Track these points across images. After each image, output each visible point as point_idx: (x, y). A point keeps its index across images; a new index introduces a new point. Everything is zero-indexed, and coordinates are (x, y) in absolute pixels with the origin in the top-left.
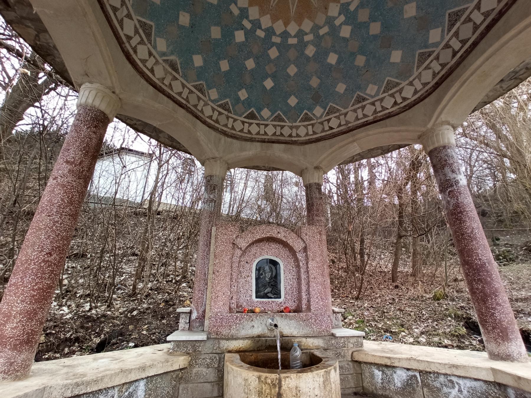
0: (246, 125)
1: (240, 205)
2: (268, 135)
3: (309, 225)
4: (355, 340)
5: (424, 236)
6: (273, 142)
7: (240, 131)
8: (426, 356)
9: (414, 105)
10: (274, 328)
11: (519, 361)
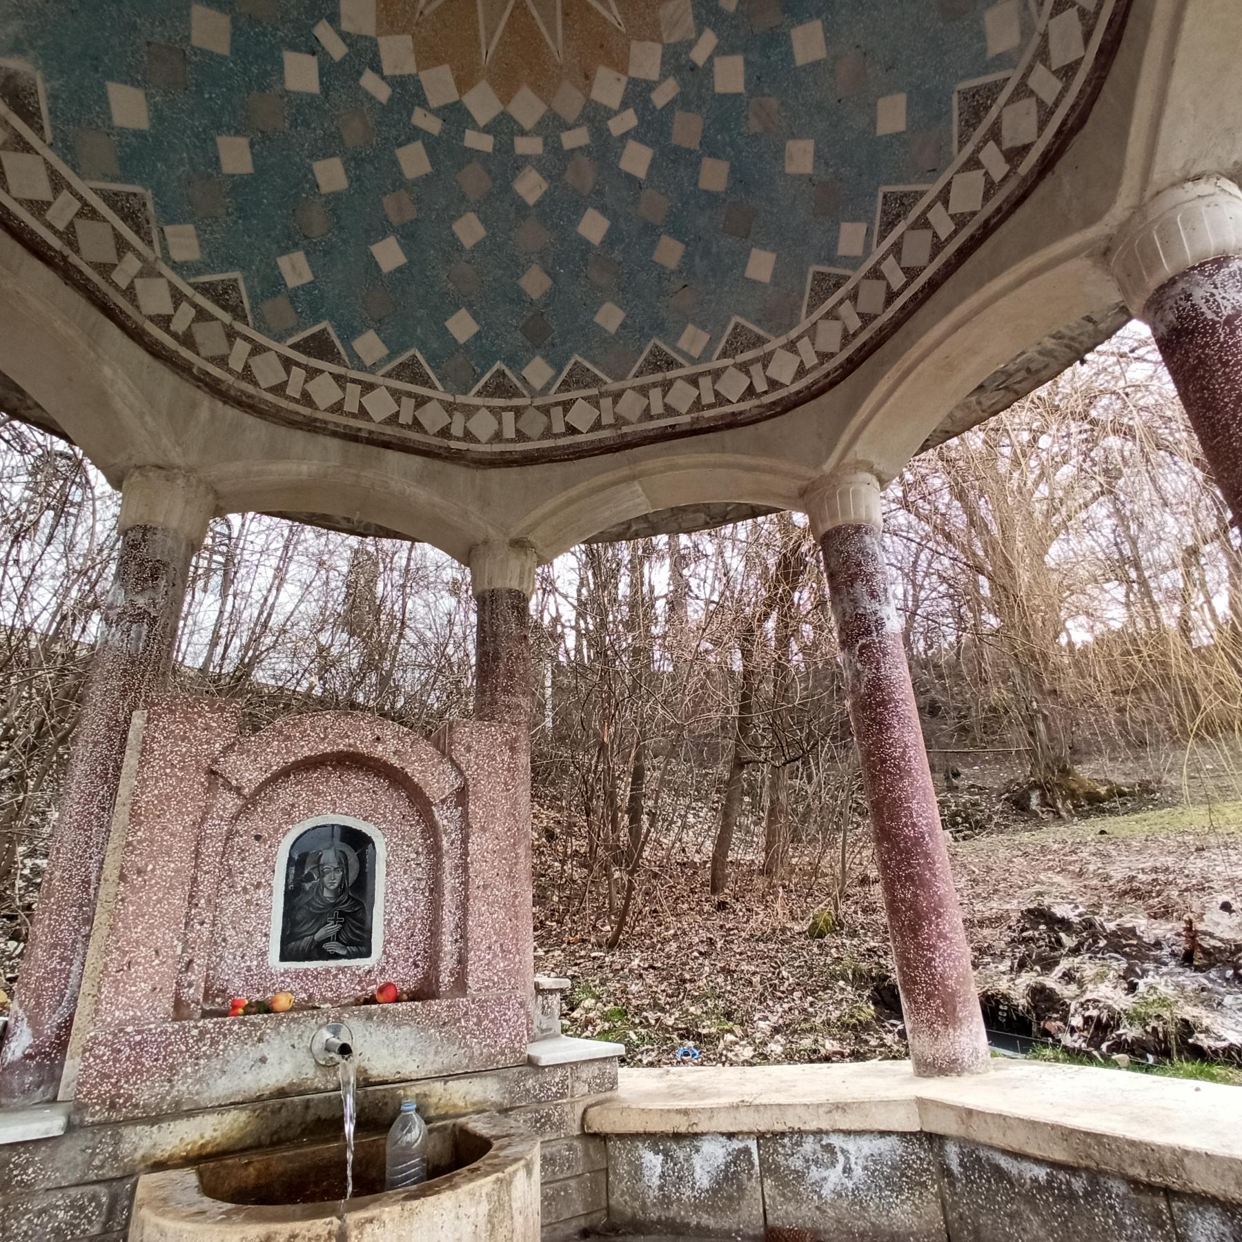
0: (298, 374)
1: (255, 639)
2: (371, 420)
3: (480, 719)
4: (594, 1069)
5: (799, 763)
6: (387, 445)
7: (271, 390)
8: (777, 1091)
9: (796, 405)
10: (338, 1058)
11: (972, 1073)
